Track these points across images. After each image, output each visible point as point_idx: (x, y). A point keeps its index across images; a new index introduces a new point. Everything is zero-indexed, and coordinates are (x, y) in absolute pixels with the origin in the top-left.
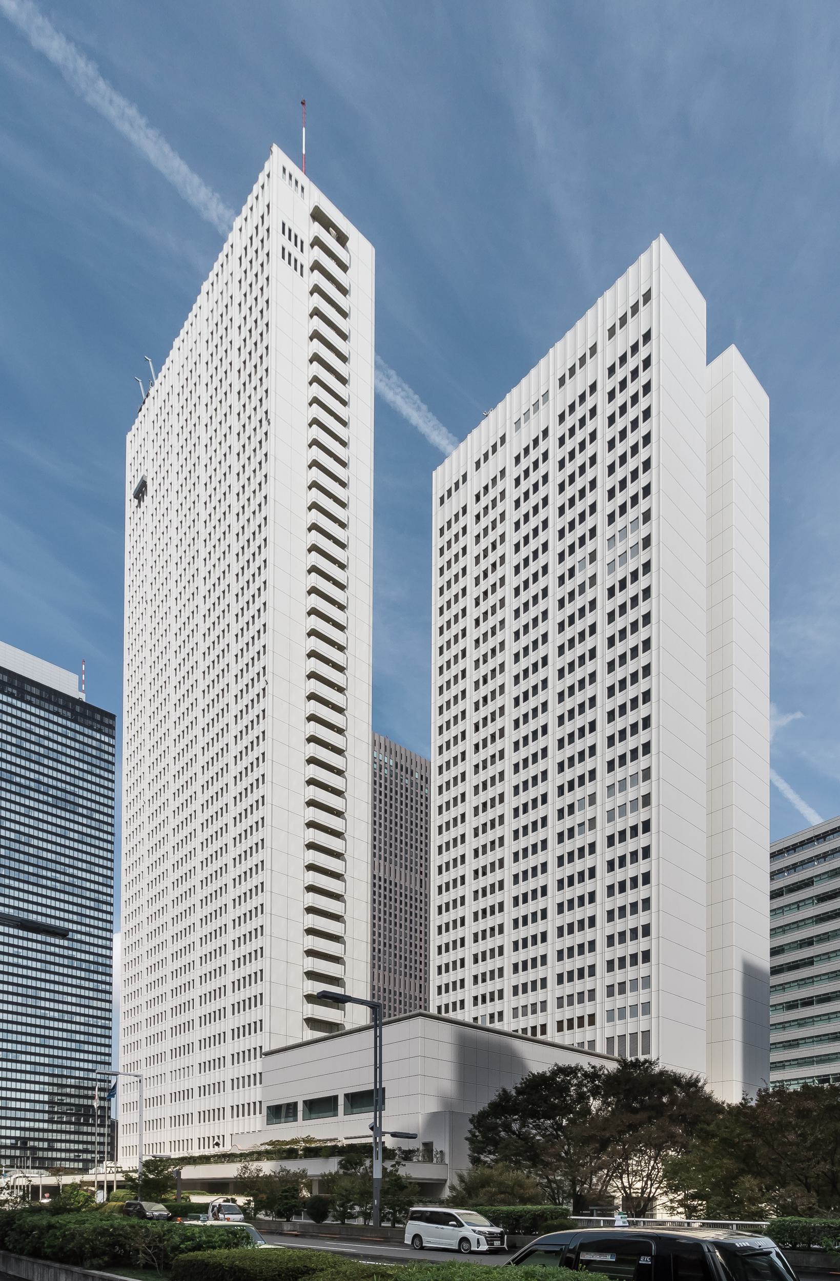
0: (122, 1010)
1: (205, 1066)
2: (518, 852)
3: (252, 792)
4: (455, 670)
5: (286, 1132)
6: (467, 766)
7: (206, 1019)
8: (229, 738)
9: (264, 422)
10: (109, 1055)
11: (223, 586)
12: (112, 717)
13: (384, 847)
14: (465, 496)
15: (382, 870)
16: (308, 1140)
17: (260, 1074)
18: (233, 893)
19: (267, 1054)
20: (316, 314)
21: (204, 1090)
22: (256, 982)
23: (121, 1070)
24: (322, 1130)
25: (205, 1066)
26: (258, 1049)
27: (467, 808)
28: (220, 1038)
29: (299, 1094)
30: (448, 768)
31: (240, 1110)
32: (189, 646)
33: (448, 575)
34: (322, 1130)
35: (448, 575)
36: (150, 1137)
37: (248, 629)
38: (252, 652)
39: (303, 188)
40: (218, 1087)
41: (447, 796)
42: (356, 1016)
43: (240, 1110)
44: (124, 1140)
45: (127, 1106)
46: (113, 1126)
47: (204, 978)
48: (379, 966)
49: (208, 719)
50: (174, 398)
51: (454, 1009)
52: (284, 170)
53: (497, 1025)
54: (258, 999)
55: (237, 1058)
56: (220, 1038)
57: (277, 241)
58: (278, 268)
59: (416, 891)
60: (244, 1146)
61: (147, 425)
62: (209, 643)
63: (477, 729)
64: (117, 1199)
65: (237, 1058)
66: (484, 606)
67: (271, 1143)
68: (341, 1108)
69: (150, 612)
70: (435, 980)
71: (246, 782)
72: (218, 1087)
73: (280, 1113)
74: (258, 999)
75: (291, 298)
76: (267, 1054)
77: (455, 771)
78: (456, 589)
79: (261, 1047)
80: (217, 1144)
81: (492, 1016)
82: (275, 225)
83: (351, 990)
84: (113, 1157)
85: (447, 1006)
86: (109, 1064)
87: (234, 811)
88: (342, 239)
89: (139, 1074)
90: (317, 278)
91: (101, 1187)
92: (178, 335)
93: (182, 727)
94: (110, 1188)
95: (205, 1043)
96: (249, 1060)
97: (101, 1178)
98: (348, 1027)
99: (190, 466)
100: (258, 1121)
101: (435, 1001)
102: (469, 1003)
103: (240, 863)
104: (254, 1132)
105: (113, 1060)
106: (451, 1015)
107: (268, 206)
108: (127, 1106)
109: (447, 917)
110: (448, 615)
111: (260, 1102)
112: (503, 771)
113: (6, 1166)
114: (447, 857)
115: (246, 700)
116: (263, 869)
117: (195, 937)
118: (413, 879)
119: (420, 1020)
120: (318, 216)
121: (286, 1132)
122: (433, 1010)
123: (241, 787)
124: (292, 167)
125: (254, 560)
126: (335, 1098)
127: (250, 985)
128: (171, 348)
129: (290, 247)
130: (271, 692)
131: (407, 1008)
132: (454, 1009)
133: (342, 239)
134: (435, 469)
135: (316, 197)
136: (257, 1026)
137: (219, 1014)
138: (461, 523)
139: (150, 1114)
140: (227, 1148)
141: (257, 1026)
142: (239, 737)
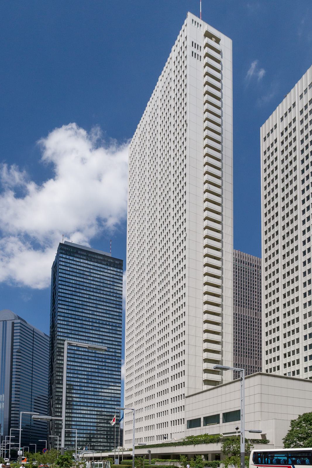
0: (125, 382)
1: (160, 404)
2: (307, 357)
3: (180, 310)
4: (273, 269)
5: (196, 432)
6: (280, 275)
7: (160, 383)
8: (169, 295)
9: (185, 125)
10: (120, 398)
11: (167, 214)
12: (122, 261)
13: (238, 302)
14: (277, 134)
15: (237, 310)
16: (206, 435)
17: (184, 406)
18: (172, 354)
19: (187, 397)
20: (207, 75)
21: (159, 414)
22: (182, 376)
23: (125, 407)
24: (212, 430)
25: (160, 404)
26: (183, 395)
27: (280, 314)
28: (166, 391)
29: (201, 414)
30: (270, 296)
31: (175, 422)
32: (153, 248)
33: (269, 198)
34: (212, 430)
35: (269, 216)
36: (138, 435)
37: (178, 258)
38: (180, 249)
39: (201, 25)
40: (165, 412)
41: (270, 309)
42: (228, 376)
43: (175, 422)
44: (125, 437)
45: (128, 423)
46: (122, 431)
47: (159, 366)
48: (239, 305)
49: (161, 271)
50: (147, 126)
51: (274, 370)
52: (193, 20)
53: (296, 376)
54: (183, 373)
55: (174, 399)
56: (166, 391)
57: (190, 49)
58: (190, 61)
59: (254, 318)
60: (176, 438)
61: (137, 140)
62: (161, 230)
63: (284, 287)
64: (124, 463)
65: (174, 399)
66: (287, 230)
67: (188, 438)
68: (221, 420)
69: (137, 215)
70: (265, 357)
71: (177, 306)
72: (165, 412)
73: (193, 423)
74: (183, 373)
75: (196, 71)
76: (187, 397)
77: (274, 307)
78: (273, 222)
79: (184, 394)
80: (165, 438)
81: (294, 372)
82: (188, 43)
83: (225, 365)
84: (121, 445)
85: (271, 369)
86: (120, 405)
87: (172, 319)
88: (218, 41)
89: (133, 408)
90: (207, 60)
91: (117, 458)
92: (149, 100)
93: (150, 283)
94: (120, 460)
95: (160, 394)
96: (179, 400)
97: (117, 453)
98: (224, 383)
99: (153, 219)
100: (183, 427)
101: (265, 367)
102: (282, 367)
103: (175, 341)
104: (181, 432)
105: (121, 403)
106: (273, 373)
107: (186, 37)
108: (128, 423)
109: (270, 347)
110: (269, 253)
111: (184, 419)
112: (298, 276)
113: (80, 449)
114: (270, 337)
115: (177, 261)
116: (184, 354)
117: (155, 356)
118: (252, 312)
119: (258, 377)
120: (208, 35)
121: (196, 432)
122: (264, 371)
123: (175, 299)
124: (196, 18)
125: (180, 228)
126: (219, 415)
127: (179, 367)
128: (146, 106)
129: (195, 51)
130: (188, 238)
131: (250, 372)
132: (274, 370)
133: (218, 41)
134: (261, 126)
135: (206, 27)
136: (182, 385)
137: (166, 381)
138: (275, 183)
139: (138, 425)
140: (169, 440)
141: (182, 385)
142: (174, 287)
